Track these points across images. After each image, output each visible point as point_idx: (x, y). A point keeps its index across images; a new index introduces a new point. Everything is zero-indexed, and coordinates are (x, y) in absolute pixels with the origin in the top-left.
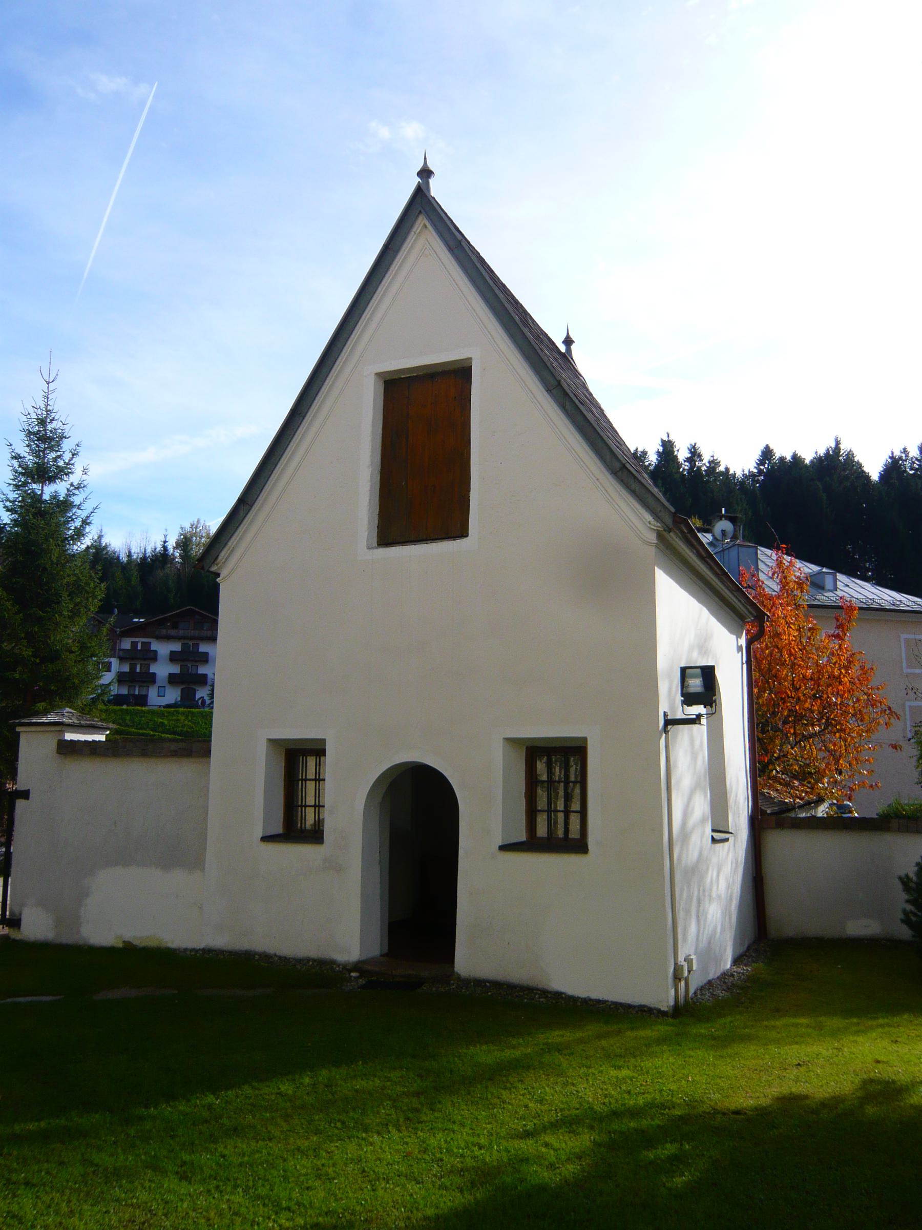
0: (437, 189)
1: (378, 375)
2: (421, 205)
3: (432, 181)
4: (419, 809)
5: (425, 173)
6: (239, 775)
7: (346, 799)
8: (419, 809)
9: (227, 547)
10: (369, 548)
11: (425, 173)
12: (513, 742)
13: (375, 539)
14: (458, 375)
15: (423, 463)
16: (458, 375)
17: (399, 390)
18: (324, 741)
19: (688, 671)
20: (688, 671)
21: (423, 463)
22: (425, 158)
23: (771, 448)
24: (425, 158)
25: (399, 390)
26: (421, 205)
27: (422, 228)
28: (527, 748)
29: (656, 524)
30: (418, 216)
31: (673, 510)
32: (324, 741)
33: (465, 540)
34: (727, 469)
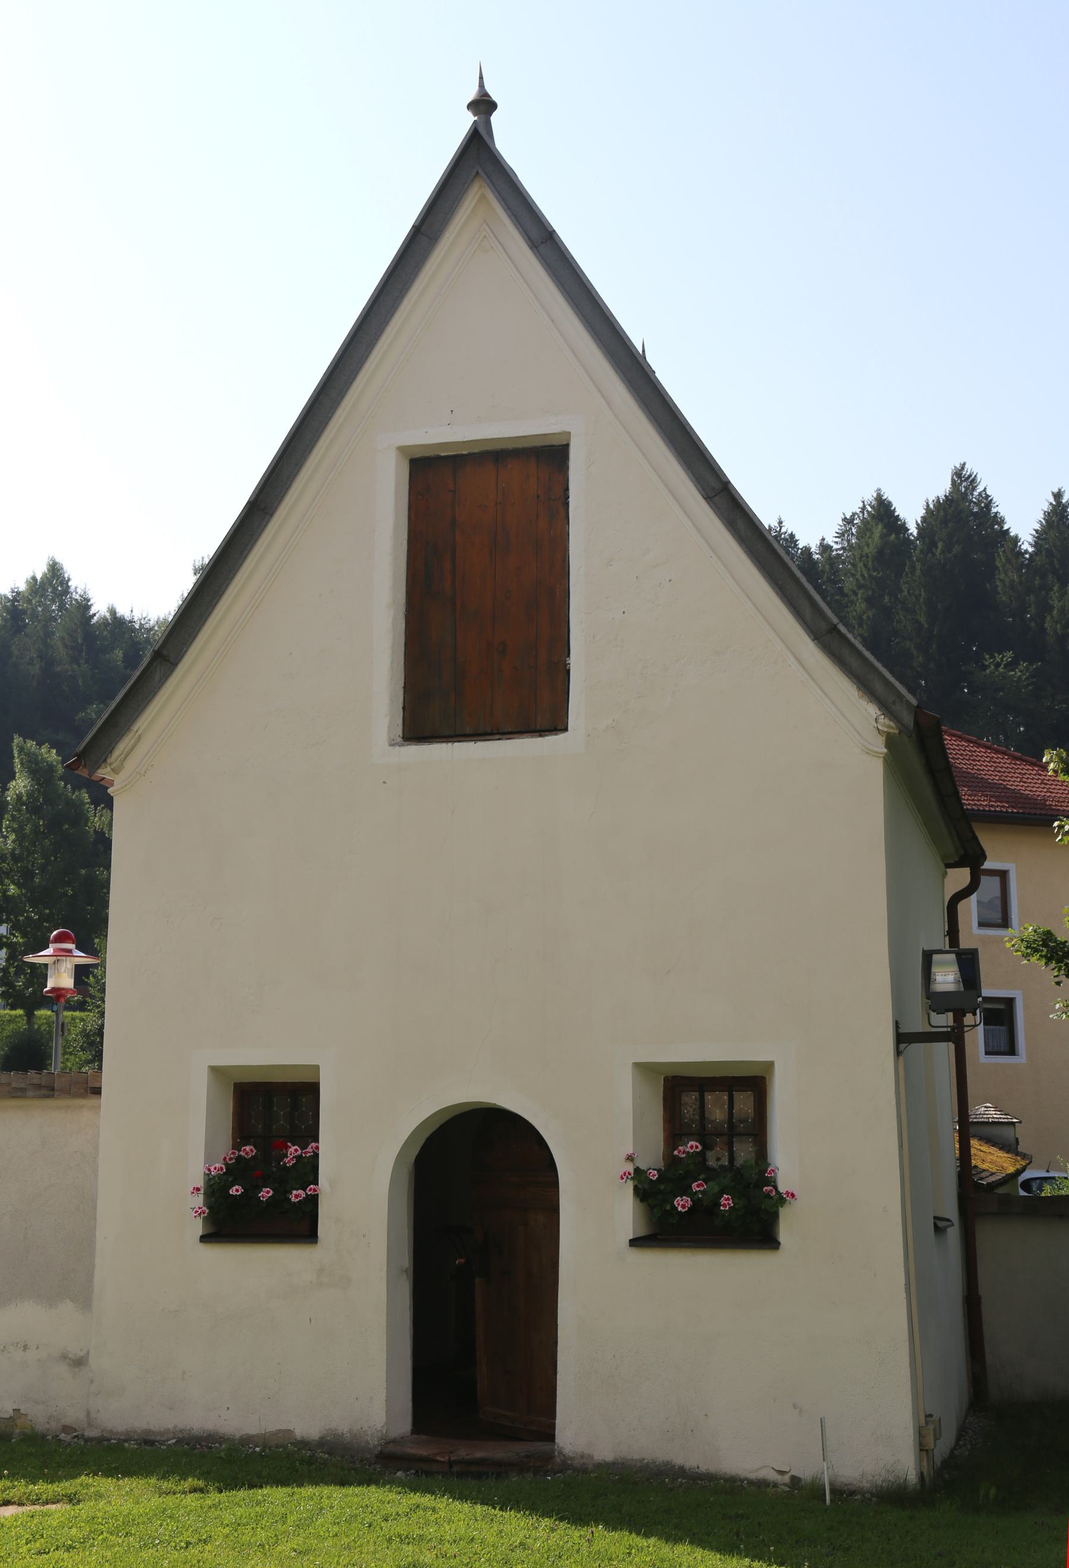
0: (508, 141)
1: (402, 450)
2: (477, 160)
3: (495, 118)
4: (479, 1185)
5: (483, 105)
6: (149, 1136)
7: (360, 1174)
8: (479, 1185)
9: (131, 734)
10: (391, 745)
11: (483, 105)
12: (645, 1069)
13: (399, 731)
14: (551, 457)
15: (484, 600)
16: (551, 457)
17: (432, 476)
18: (316, 1068)
19: (935, 957)
20: (935, 957)
21: (484, 600)
22: (481, 78)
23: (57, 560)
24: (481, 78)
25: (432, 476)
26: (477, 160)
27: (478, 201)
28: (666, 1080)
29: (887, 722)
30: (473, 180)
31: (914, 702)
32: (316, 1068)
33: (561, 737)
34: (113, 612)
